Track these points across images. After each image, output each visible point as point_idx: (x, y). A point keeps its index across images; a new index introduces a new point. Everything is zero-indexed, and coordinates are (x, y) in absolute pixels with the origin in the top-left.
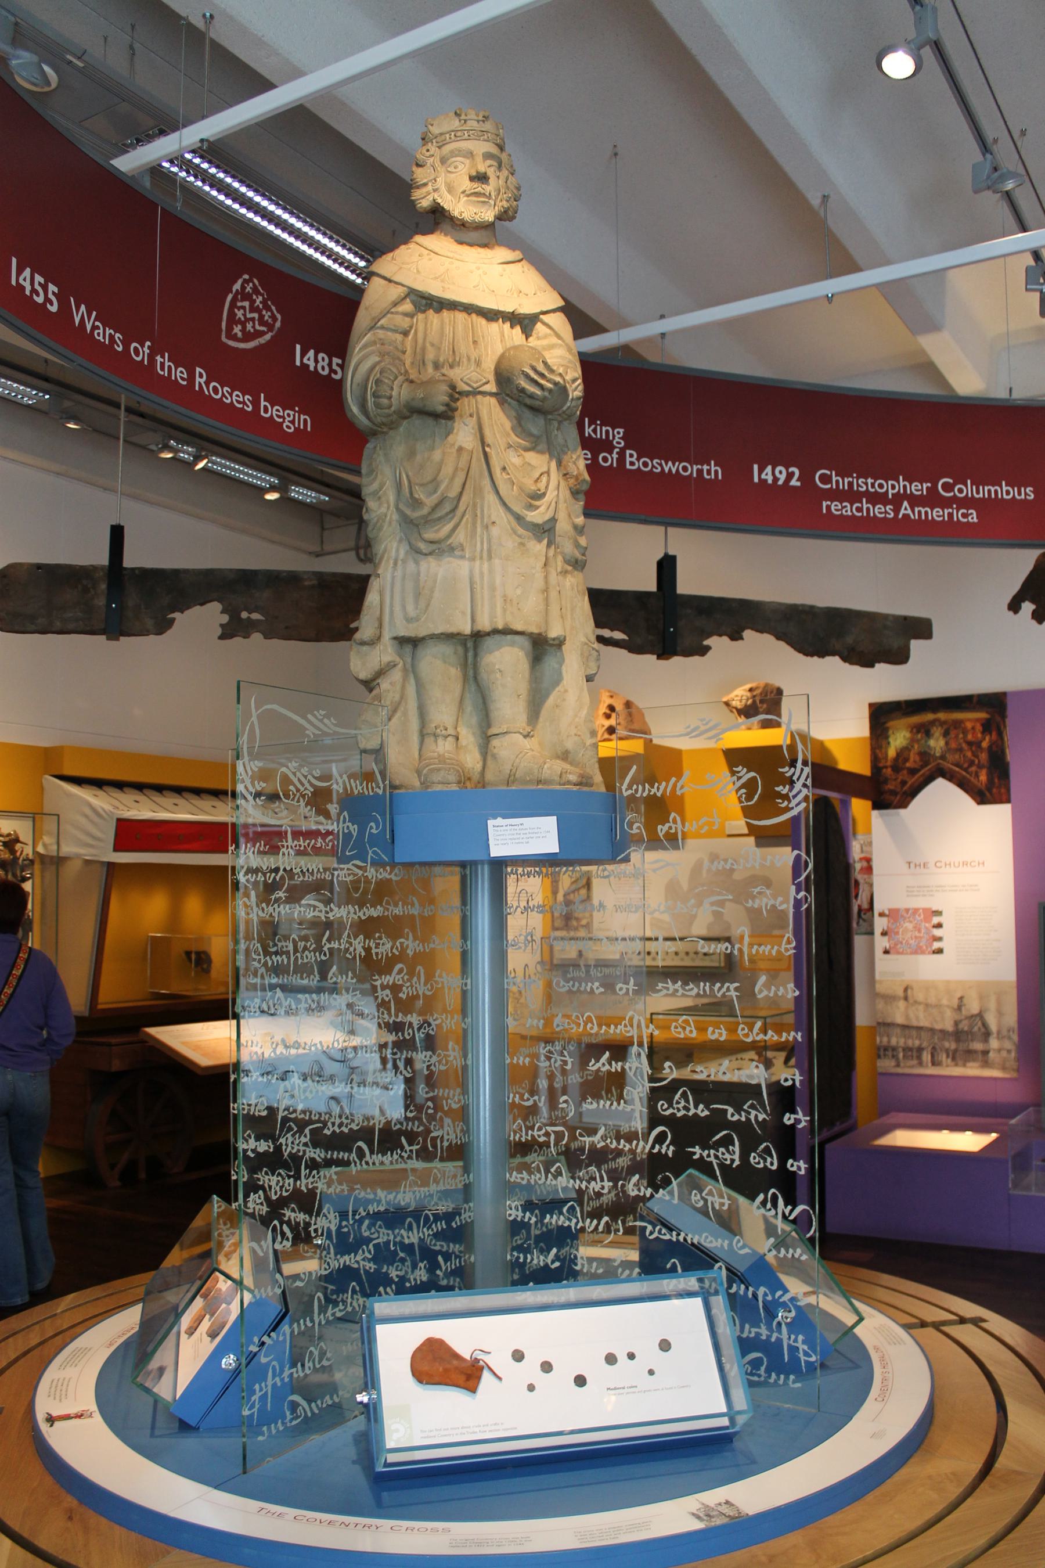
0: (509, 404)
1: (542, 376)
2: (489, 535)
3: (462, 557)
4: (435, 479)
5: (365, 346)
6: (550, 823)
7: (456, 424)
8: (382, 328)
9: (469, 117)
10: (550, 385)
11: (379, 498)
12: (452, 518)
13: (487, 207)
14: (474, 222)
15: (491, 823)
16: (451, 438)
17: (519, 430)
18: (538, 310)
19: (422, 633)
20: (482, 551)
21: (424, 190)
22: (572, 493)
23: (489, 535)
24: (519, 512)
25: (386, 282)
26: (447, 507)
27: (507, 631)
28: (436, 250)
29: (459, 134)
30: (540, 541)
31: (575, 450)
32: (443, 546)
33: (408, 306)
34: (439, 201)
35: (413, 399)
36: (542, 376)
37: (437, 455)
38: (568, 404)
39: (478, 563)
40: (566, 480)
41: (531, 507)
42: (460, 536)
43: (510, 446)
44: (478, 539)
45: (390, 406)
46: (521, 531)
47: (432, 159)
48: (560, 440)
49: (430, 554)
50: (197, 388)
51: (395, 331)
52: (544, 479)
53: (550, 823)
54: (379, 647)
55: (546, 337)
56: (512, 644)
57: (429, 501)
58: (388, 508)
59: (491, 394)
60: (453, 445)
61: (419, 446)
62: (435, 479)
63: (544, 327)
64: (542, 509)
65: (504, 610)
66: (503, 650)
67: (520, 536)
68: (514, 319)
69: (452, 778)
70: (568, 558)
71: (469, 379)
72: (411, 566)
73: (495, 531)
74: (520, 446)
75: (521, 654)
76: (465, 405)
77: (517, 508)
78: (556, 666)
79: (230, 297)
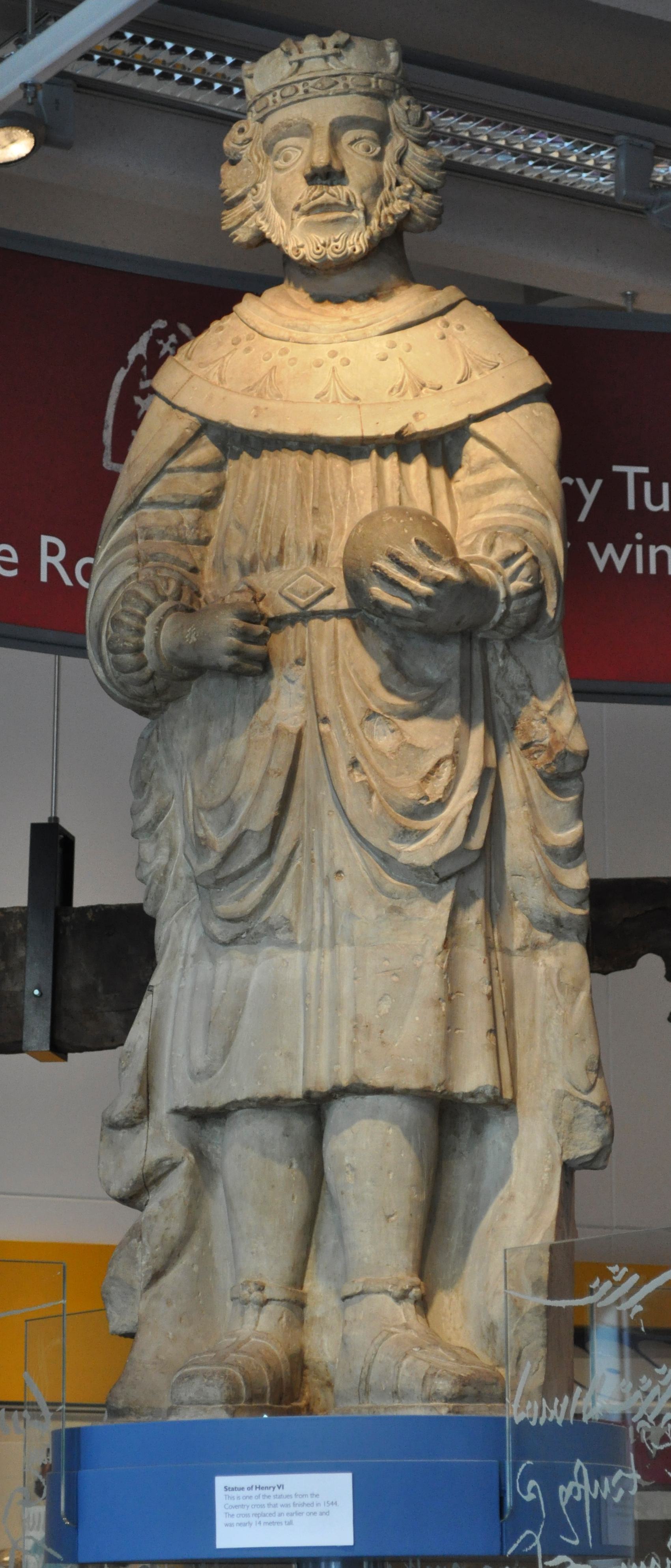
0: (376, 628)
1: (411, 571)
2: (331, 897)
3: (291, 944)
4: (229, 797)
5: (116, 547)
6: (340, 1484)
7: (275, 683)
8: (152, 503)
9: (306, 53)
10: (425, 589)
11: (157, 836)
12: (267, 870)
13: (346, 228)
14: (325, 261)
15: (221, 1482)
16: (264, 711)
17: (395, 677)
18: (460, 416)
19: (219, 1100)
20: (322, 930)
21: (238, 211)
22: (546, 780)
23: (331, 897)
24: (383, 848)
25: (169, 407)
26: (252, 850)
27: (358, 1089)
28: (262, 328)
29: (288, 91)
30: (435, 900)
31: (551, 690)
32: (257, 924)
33: (205, 451)
34: (265, 228)
35: (180, 647)
36: (411, 571)
37: (238, 746)
38: (501, 609)
39: (315, 953)
40: (529, 756)
41: (406, 834)
42: (284, 904)
43: (371, 715)
44: (316, 905)
45: (142, 666)
46: (391, 883)
47: (248, 147)
48: (515, 674)
49: (234, 941)
50: (44, 578)
51: (181, 505)
52: (446, 771)
53: (340, 1484)
54: (147, 1131)
55: (484, 465)
56: (374, 1114)
57: (221, 841)
58: (171, 855)
59: (338, 614)
60: (266, 724)
61: (214, 732)
62: (229, 797)
63: (480, 446)
64: (433, 836)
65: (354, 1047)
66: (356, 1127)
67: (390, 895)
68: (403, 445)
69: (215, 1392)
70: (537, 916)
71: (292, 590)
72: (206, 965)
73: (342, 888)
74: (394, 711)
75: (393, 1132)
76: (286, 644)
77: (377, 841)
78: (504, 1144)
79: (121, 376)
